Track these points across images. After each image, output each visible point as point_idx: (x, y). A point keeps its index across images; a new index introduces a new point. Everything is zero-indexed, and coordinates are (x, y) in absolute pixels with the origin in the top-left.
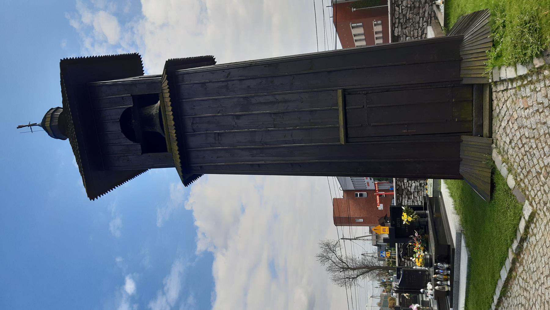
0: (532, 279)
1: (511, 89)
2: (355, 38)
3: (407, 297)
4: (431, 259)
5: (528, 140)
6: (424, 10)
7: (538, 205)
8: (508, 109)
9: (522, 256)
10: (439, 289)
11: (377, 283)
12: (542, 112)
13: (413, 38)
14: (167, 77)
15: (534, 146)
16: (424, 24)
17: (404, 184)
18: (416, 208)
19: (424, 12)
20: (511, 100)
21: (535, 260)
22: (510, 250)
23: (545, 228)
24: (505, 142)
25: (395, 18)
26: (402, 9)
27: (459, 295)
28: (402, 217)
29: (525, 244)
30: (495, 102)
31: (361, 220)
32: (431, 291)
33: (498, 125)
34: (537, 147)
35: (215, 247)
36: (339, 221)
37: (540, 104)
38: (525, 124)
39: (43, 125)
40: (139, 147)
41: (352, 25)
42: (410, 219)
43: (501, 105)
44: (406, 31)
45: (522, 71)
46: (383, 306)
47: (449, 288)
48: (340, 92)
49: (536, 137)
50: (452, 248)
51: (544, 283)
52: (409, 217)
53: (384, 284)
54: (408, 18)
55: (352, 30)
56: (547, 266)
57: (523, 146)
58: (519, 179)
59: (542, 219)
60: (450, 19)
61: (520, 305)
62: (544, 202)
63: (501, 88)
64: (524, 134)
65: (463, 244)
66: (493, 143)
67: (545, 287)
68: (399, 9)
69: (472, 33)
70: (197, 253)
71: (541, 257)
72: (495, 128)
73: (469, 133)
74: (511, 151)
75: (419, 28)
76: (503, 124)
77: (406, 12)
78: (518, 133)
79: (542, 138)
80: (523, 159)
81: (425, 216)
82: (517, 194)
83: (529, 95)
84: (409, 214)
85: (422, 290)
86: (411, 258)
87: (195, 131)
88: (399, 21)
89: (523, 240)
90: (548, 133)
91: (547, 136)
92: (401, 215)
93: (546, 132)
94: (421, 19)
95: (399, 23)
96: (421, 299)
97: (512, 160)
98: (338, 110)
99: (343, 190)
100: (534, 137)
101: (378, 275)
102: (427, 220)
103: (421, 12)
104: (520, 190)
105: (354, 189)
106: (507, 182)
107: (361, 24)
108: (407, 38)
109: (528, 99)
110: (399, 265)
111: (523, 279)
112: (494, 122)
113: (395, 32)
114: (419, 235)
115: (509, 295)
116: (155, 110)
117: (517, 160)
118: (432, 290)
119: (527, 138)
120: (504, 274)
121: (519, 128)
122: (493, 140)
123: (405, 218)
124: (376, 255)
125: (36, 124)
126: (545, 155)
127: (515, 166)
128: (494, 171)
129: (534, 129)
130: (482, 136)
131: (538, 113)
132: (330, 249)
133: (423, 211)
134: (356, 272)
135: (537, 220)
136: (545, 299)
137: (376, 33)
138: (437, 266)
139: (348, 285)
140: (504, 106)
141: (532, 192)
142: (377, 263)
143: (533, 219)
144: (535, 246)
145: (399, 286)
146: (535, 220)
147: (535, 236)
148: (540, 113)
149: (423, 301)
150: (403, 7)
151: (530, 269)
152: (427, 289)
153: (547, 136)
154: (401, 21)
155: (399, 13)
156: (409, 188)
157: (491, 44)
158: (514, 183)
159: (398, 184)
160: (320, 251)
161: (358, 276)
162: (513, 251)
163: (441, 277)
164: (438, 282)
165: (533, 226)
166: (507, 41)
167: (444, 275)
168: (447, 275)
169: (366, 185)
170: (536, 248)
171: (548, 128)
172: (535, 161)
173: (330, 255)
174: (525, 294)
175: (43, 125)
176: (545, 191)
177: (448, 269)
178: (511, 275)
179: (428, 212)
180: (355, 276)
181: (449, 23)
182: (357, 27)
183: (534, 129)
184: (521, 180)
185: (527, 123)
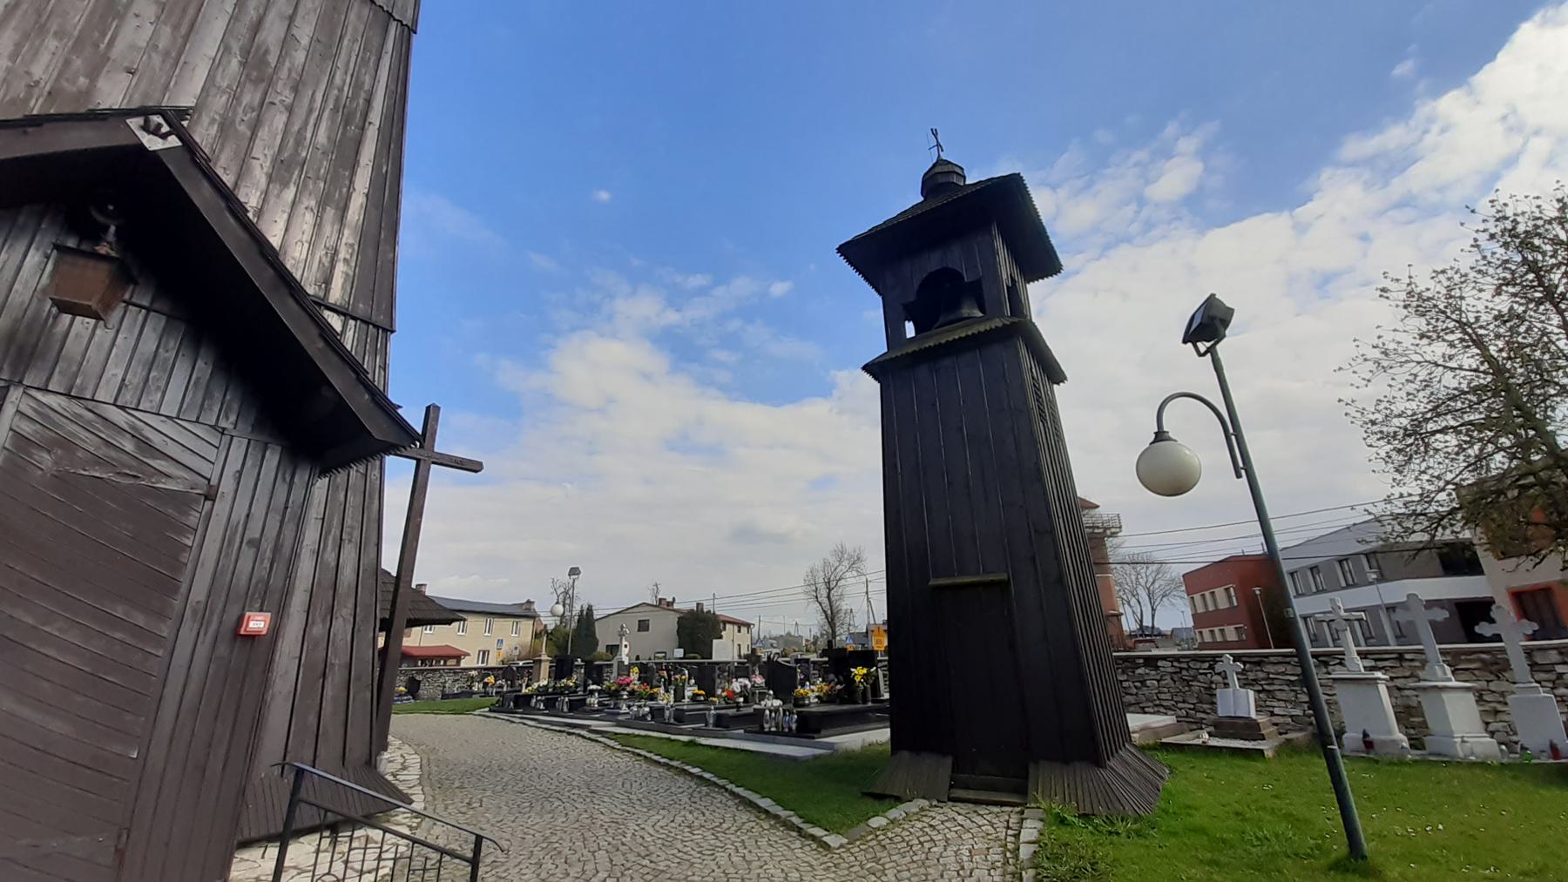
0: (749, 838)
1: (1006, 832)
2: (1207, 594)
4: (804, 706)
5: (927, 850)
6: (1209, 711)
7: (838, 856)
8: (980, 827)
9: (781, 829)
12: (958, 874)
13: (1157, 691)
14: (1007, 325)
15: (915, 858)
16: (1183, 711)
19: (1204, 712)
20: (990, 832)
21: (771, 845)
22: (792, 813)
23: (806, 862)
24: (934, 818)
25: (1188, 662)
26: (1205, 674)
29: (794, 834)
30: (996, 809)
33: (961, 811)
34: (913, 861)
35: (840, 398)
37: (971, 873)
38: (949, 849)
39: (940, 162)
40: (912, 299)
41: (1232, 589)
42: (858, 679)
43: (988, 817)
44: (1168, 680)
45: (1025, 852)
47: (767, 730)
48: (1004, 577)
49: (927, 861)
51: (738, 852)
54: (1190, 683)
55: (1222, 589)
56: (757, 859)
57: (921, 843)
58: (878, 833)
59: (819, 859)
60: (1176, 753)
61: (722, 821)
62: (839, 864)
63: (1014, 819)
64: (936, 846)
65: (818, 751)
66: (939, 801)
67: (732, 854)
68: (1204, 669)
69: (1110, 783)
70: (833, 372)
71: (771, 853)
72: (960, 807)
73: (956, 769)
74: (919, 825)
75: (1176, 702)
76: (960, 818)
77: (1202, 680)
78: (940, 837)
79: (922, 870)
80: (904, 841)
81: (865, 701)
82: (860, 829)
83: (989, 857)
86: (820, 679)
87: (936, 371)
88: (1184, 669)
89: (799, 830)
90: (927, 880)
91: (924, 878)
92: (864, 667)
93: (929, 877)
94: (1192, 706)
95: (1181, 669)
97: (906, 827)
98: (978, 573)
100: (927, 859)
102: (859, 704)
103: (1205, 706)
104: (863, 834)
106: (878, 815)
107: (1235, 604)
108: (1155, 682)
109: (983, 857)
111: (753, 828)
112: (971, 805)
113: (1164, 662)
115: (740, 808)
116: (968, 311)
117: (905, 833)
118: (772, 705)
119: (929, 849)
120: (765, 803)
121: (947, 840)
122: (944, 802)
123: (859, 672)
125: (942, 150)
126: (899, 871)
127: (897, 829)
128: (898, 800)
129: (938, 860)
130: (951, 787)
131: (959, 868)
132: (854, 563)
133: (870, 698)
134: (826, 601)
135: (820, 852)
136: (718, 852)
137: (1222, 631)
140: (986, 822)
141: (858, 849)
143: (822, 847)
144: (788, 846)
146: (820, 849)
147: (801, 848)
148: (958, 872)
150: (1209, 676)
151: (762, 837)
153: (924, 878)
154: (1184, 672)
155: (1197, 669)
157: (1088, 811)
158: (874, 826)
160: (849, 548)
161: (820, 604)
162: (790, 816)
163: (780, 718)
164: (773, 715)
165: (814, 846)
166: (1082, 836)
168: (783, 728)
170: (785, 848)
171: (934, 881)
172: (894, 858)
173: (846, 563)
174: (734, 828)
175: (940, 162)
176: (852, 866)
177: (790, 729)
178: (763, 813)
179: (870, 704)
180: (819, 600)
181: (1167, 751)
182: (1230, 597)
183: (938, 860)
184: (877, 836)
185: (950, 852)
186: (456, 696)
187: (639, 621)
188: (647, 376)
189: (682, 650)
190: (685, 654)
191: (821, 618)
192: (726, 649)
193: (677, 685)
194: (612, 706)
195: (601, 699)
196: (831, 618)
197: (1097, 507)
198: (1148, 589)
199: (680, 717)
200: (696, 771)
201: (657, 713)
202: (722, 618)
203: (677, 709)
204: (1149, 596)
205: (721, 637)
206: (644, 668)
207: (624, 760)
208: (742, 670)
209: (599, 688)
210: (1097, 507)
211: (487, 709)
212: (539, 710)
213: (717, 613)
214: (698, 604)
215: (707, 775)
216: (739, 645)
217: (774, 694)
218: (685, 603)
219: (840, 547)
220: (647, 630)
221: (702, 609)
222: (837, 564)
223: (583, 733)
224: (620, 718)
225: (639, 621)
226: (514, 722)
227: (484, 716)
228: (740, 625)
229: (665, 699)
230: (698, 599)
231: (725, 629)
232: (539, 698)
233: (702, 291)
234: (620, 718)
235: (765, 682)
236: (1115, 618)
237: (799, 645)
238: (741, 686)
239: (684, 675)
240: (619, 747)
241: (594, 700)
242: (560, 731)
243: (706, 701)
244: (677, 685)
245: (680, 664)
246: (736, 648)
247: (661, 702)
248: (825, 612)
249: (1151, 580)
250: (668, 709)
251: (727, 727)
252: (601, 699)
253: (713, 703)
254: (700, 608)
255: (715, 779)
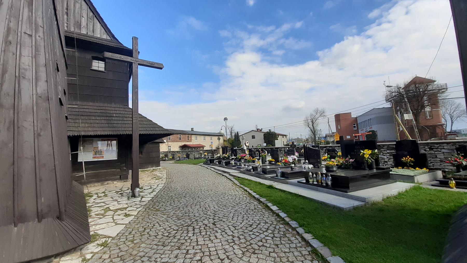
3: (302, 151)
10: (310, 175)
11: (307, 137)
17: (385, 150)
18: (377, 161)
27: (308, 189)
28: (367, 150)
31: (339, 128)
32: (307, 167)
36: (338, 117)
42: (367, 156)
46: (298, 140)
47: (311, 183)
50: (348, 191)
52: (369, 155)
53: (307, 140)
84: (371, 155)
85: (307, 161)
96: (301, 159)
99: (357, 117)
101: (311, 137)
105: (358, 123)
110: (321, 147)
114: (352, 162)
123: (367, 153)
124: (321, 136)
133: (375, 167)
134: (312, 127)
138: (329, 176)
139: (305, 124)
142: (317, 136)
145: (308, 147)
149: (301, 160)
152: (308, 164)
156: (382, 154)
159: (385, 146)
161: (310, 128)
164: (315, 175)
167: (321, 180)
168: (322, 183)
169: (362, 129)
177: (327, 184)
179: (375, 171)
180: (309, 127)
186: (198, 158)
187: (252, 136)
188: (254, 64)
189: (266, 144)
190: (267, 145)
191: (310, 133)
192: (279, 143)
193: (263, 157)
194: (239, 165)
195: (235, 162)
196: (314, 132)
197: (436, 81)
198: (451, 115)
199: (265, 171)
200: (274, 208)
201: (255, 169)
202: (278, 134)
203: (263, 168)
204: (451, 117)
205: (278, 139)
206: (250, 150)
207: (238, 192)
208: (290, 152)
209: (235, 157)
210: (436, 81)
211: (202, 163)
212: (217, 164)
213: (276, 132)
214: (269, 130)
215: (283, 215)
216: (284, 142)
217: (308, 162)
218: (265, 130)
219: (316, 109)
220: (255, 138)
221: (271, 131)
222: (315, 114)
223: (227, 175)
224: (241, 170)
225: (252, 136)
226: (208, 168)
227: (201, 166)
228: (283, 135)
229: (258, 163)
230: (270, 129)
231: (278, 137)
232: (216, 160)
233: (272, 32)
234: (241, 170)
235: (299, 155)
236: (441, 126)
237: (302, 141)
238: (292, 159)
239: (265, 153)
240: (239, 184)
241: (233, 162)
242: (220, 174)
243: (275, 164)
244: (263, 157)
245: (264, 148)
246: (282, 142)
247: (256, 164)
248: (311, 130)
249: (452, 111)
250: (259, 168)
251: (287, 178)
252: (235, 162)
253: (279, 165)
254: (270, 131)
255: (287, 219)
